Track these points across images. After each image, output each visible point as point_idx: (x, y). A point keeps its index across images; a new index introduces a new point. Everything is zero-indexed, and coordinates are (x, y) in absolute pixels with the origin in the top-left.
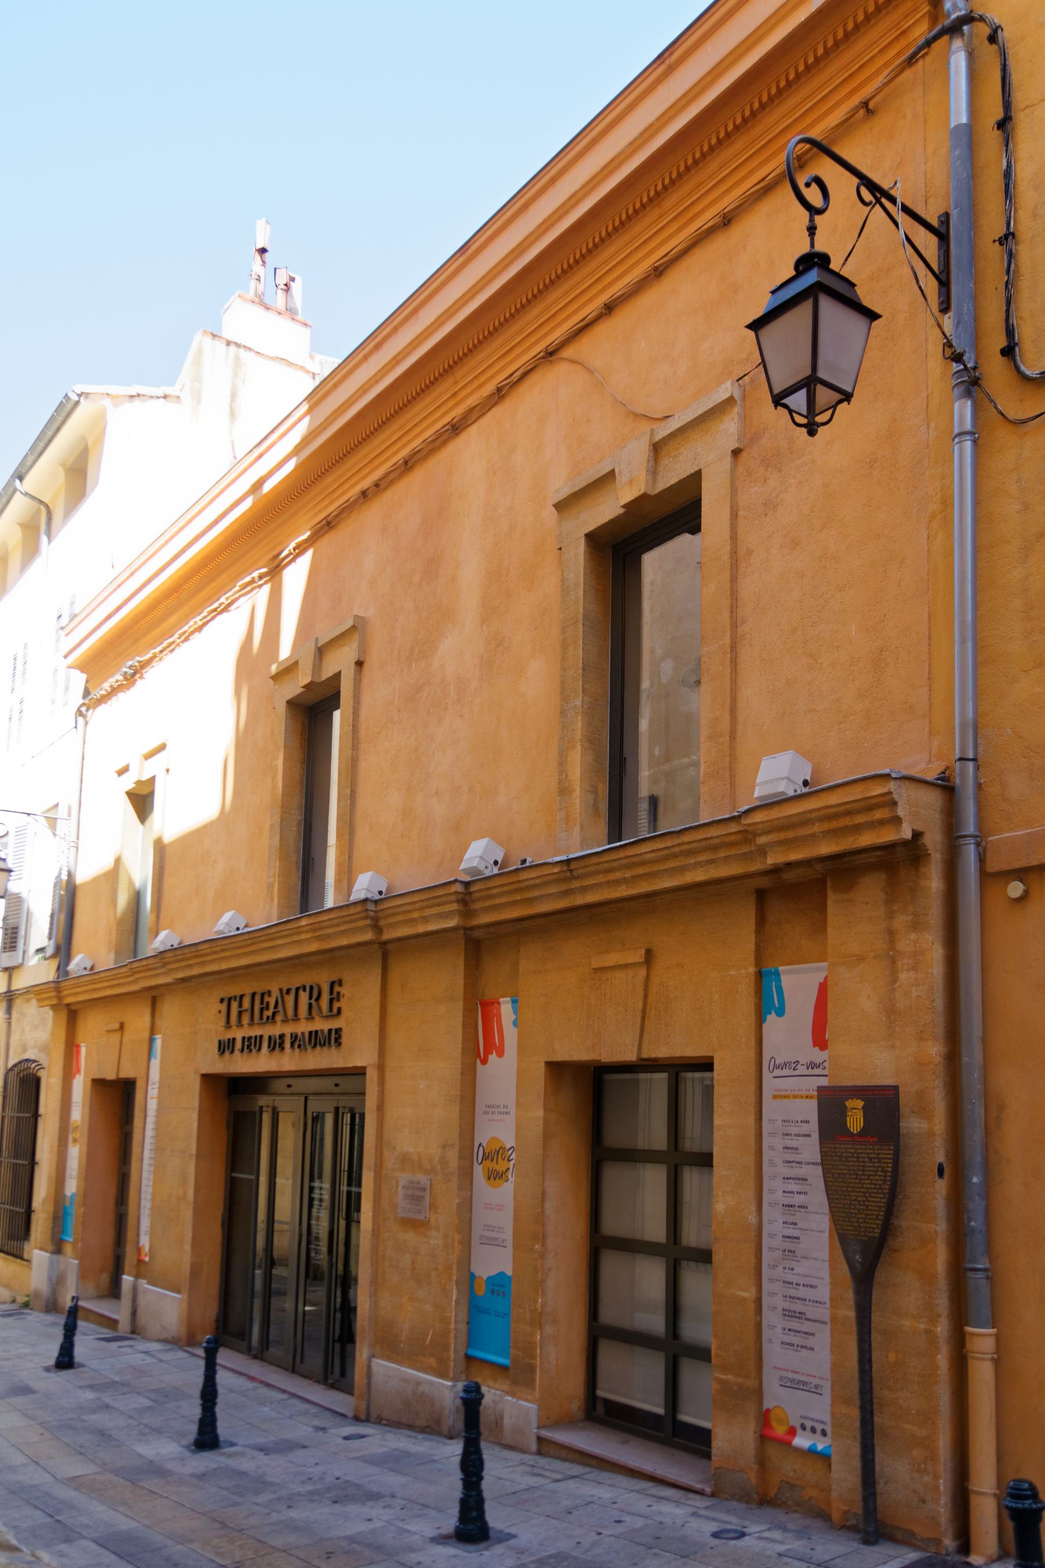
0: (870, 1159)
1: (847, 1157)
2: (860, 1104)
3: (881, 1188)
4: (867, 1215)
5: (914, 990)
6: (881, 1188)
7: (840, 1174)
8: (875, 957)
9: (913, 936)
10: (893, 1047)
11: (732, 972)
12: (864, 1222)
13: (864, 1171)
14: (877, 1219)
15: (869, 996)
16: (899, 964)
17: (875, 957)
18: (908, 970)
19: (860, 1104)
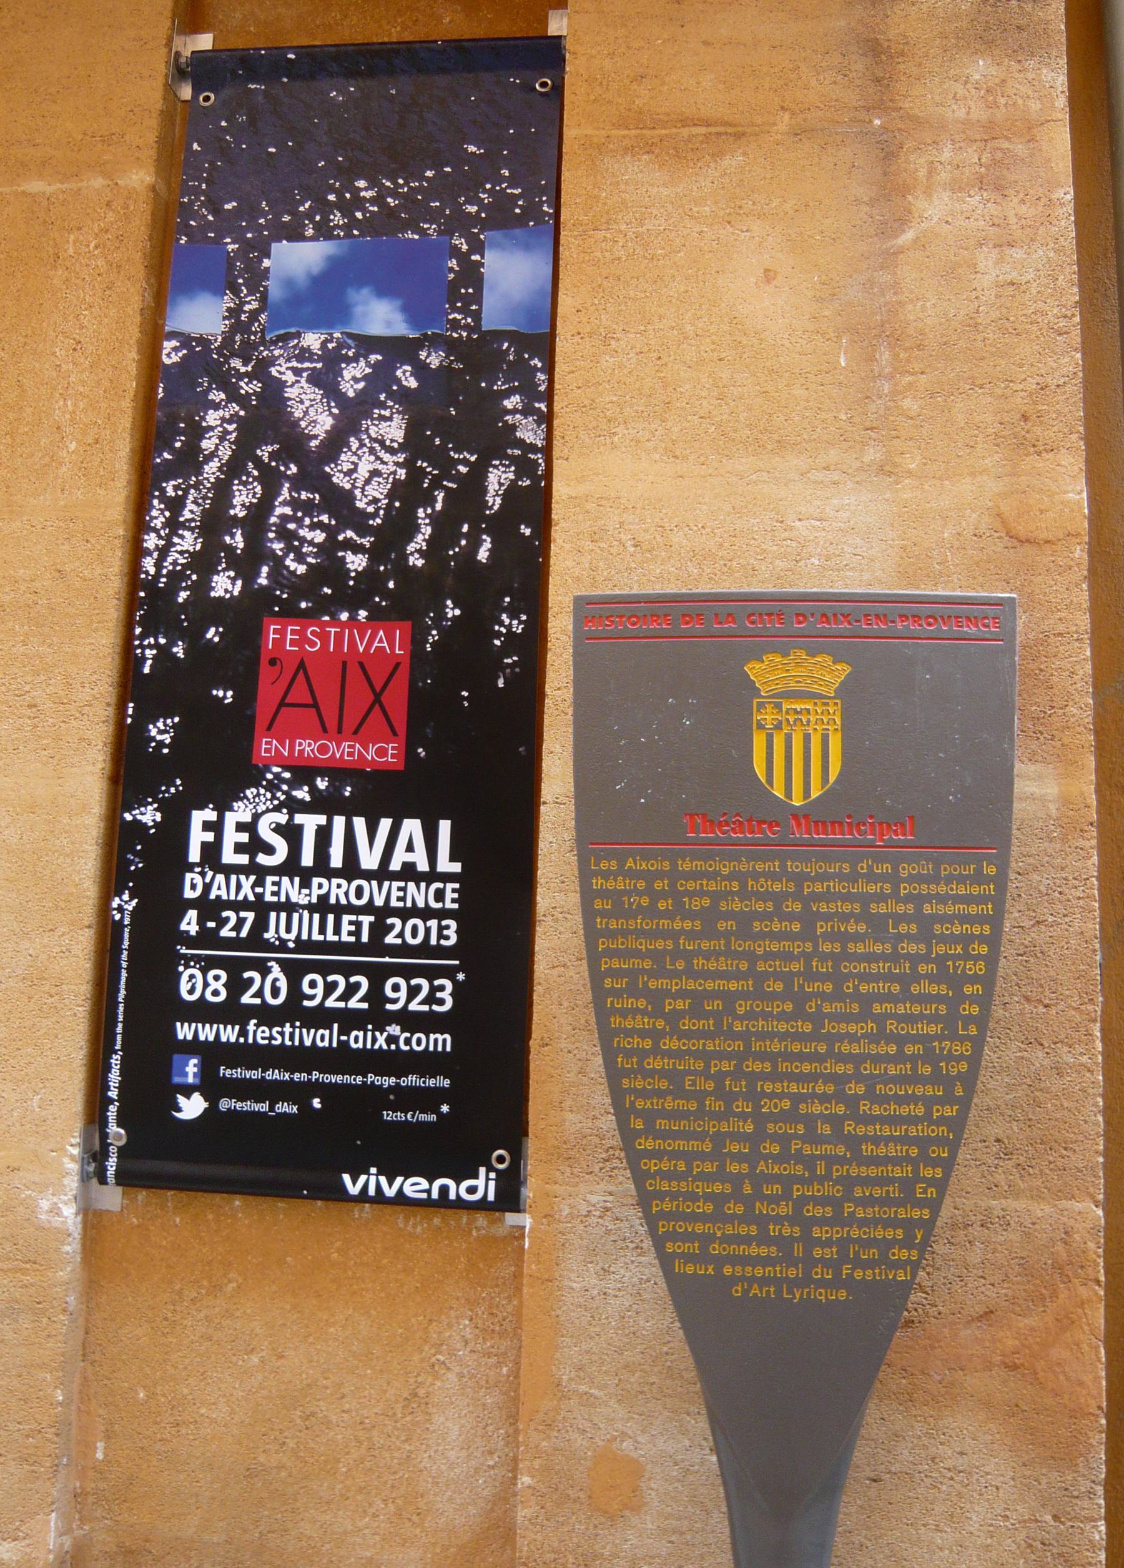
0: (878, 925)
1: (745, 920)
2: (830, 674)
3: (930, 1057)
4: (849, 1183)
5: (986, 259)
6: (930, 1057)
7: (699, 998)
8: (798, 133)
9: (981, 68)
10: (886, 469)
11: (36, 186)
12: (838, 1220)
13: (837, 978)
14: (213, 1055)
15: (769, 276)
16: (917, 163)
17: (798, 133)
18: (957, 187)
19: (830, 674)
